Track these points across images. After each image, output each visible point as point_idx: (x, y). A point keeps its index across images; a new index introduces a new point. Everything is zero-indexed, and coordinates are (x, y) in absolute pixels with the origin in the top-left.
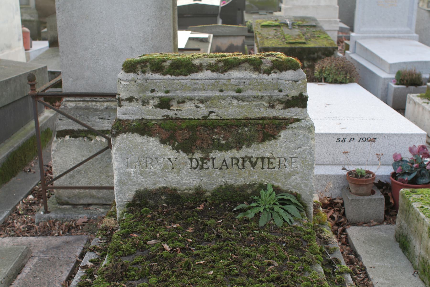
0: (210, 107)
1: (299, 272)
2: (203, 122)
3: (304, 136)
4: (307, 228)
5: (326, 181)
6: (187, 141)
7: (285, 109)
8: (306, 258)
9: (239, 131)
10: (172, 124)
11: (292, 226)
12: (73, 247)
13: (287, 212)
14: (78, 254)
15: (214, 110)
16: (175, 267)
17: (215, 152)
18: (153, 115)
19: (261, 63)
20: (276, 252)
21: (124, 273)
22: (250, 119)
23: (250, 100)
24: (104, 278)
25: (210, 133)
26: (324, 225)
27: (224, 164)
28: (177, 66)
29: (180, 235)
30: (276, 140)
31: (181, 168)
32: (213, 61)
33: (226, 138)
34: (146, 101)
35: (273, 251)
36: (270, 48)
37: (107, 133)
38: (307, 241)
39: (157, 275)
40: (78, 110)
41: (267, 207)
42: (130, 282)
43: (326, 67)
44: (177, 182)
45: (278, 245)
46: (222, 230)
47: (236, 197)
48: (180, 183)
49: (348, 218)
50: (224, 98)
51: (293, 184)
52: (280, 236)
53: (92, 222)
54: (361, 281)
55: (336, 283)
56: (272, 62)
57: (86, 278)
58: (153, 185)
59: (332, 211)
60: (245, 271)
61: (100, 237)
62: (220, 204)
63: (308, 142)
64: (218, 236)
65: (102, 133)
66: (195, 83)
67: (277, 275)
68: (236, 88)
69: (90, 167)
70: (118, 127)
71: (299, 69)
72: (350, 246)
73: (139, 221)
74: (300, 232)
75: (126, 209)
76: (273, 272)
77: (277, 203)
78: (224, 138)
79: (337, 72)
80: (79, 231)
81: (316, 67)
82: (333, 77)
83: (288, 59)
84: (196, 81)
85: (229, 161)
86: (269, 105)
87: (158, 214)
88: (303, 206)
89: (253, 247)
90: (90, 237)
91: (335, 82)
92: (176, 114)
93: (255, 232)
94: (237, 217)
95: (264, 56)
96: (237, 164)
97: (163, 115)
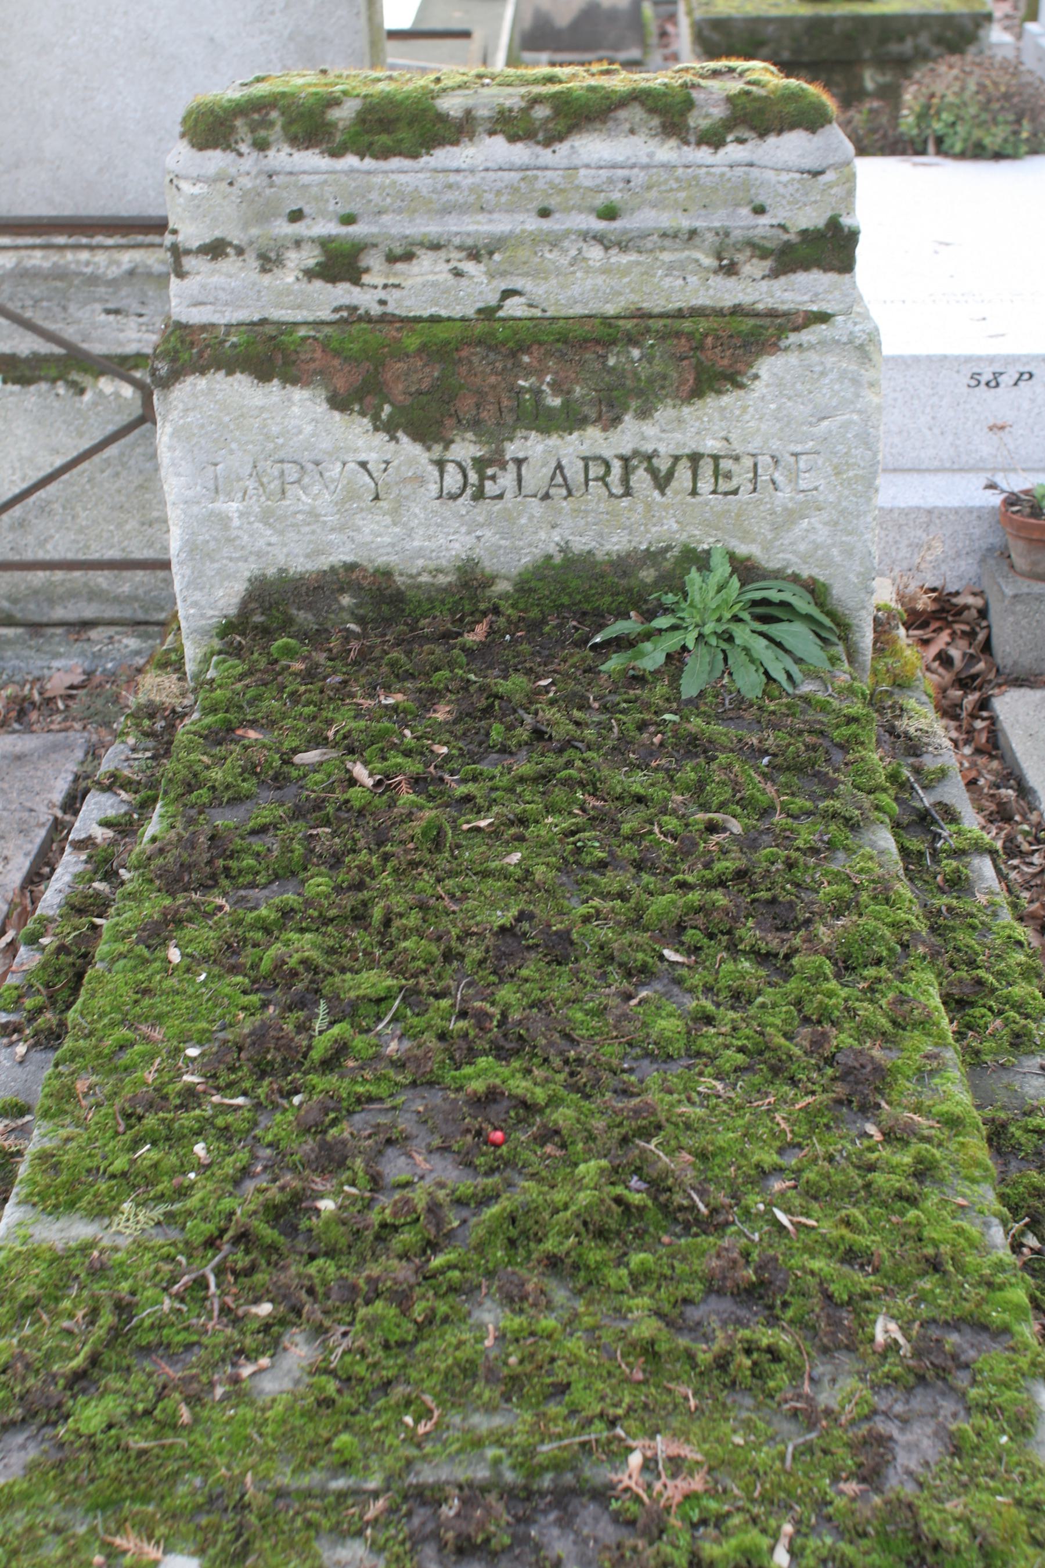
0: (503, 274)
1: (814, 851)
2: (480, 328)
3: (843, 375)
4: (846, 703)
5: (926, 530)
6: (424, 399)
7: (777, 277)
8: (837, 804)
9: (611, 362)
10: (369, 337)
11: (795, 696)
12: (39, 774)
13: (779, 645)
14: (58, 797)
15: (518, 283)
16: (391, 839)
17: (526, 438)
18: (299, 307)
19: (689, 104)
20: (736, 786)
21: (221, 862)
22: (650, 316)
23: (650, 246)
24: (151, 881)
25: (504, 369)
26: (909, 687)
27: (559, 480)
28: (380, 121)
29: (407, 732)
30: (742, 393)
31: (406, 498)
32: (512, 98)
33: (565, 388)
34: (273, 255)
35: (724, 784)
36: (736, 20)
37: (136, 367)
38: (843, 747)
39: (331, 867)
40: (26, 281)
41: (707, 629)
42: (242, 893)
43: (943, 97)
44: (393, 545)
45: (745, 762)
46: (551, 714)
47: (602, 594)
48: (403, 550)
49: (999, 661)
50: (555, 241)
51: (802, 547)
52: (750, 730)
53: (100, 685)
54: (1034, 876)
55: (939, 888)
56: (730, 99)
57: (91, 880)
58: (307, 556)
59: (944, 637)
60: (629, 850)
61: (131, 741)
62: (544, 622)
63: (858, 396)
64: (538, 734)
65: (120, 366)
66: (450, 186)
67: (738, 864)
68: (600, 201)
69: (84, 491)
70: (176, 352)
71: (828, 127)
72: (1002, 758)
73: (265, 684)
74: (821, 717)
75: (217, 644)
76: (724, 852)
77: (746, 616)
78: (557, 387)
79: (984, 116)
80: (58, 718)
81: (908, 97)
82: (969, 133)
83: (786, 87)
84: (453, 178)
85: (574, 471)
86: (716, 263)
87: (330, 659)
88: (838, 625)
89: (657, 769)
90: (94, 738)
91: (977, 152)
92: (382, 302)
93: (667, 717)
94: (602, 668)
95: (702, 76)
96: (602, 479)
97: (335, 304)
